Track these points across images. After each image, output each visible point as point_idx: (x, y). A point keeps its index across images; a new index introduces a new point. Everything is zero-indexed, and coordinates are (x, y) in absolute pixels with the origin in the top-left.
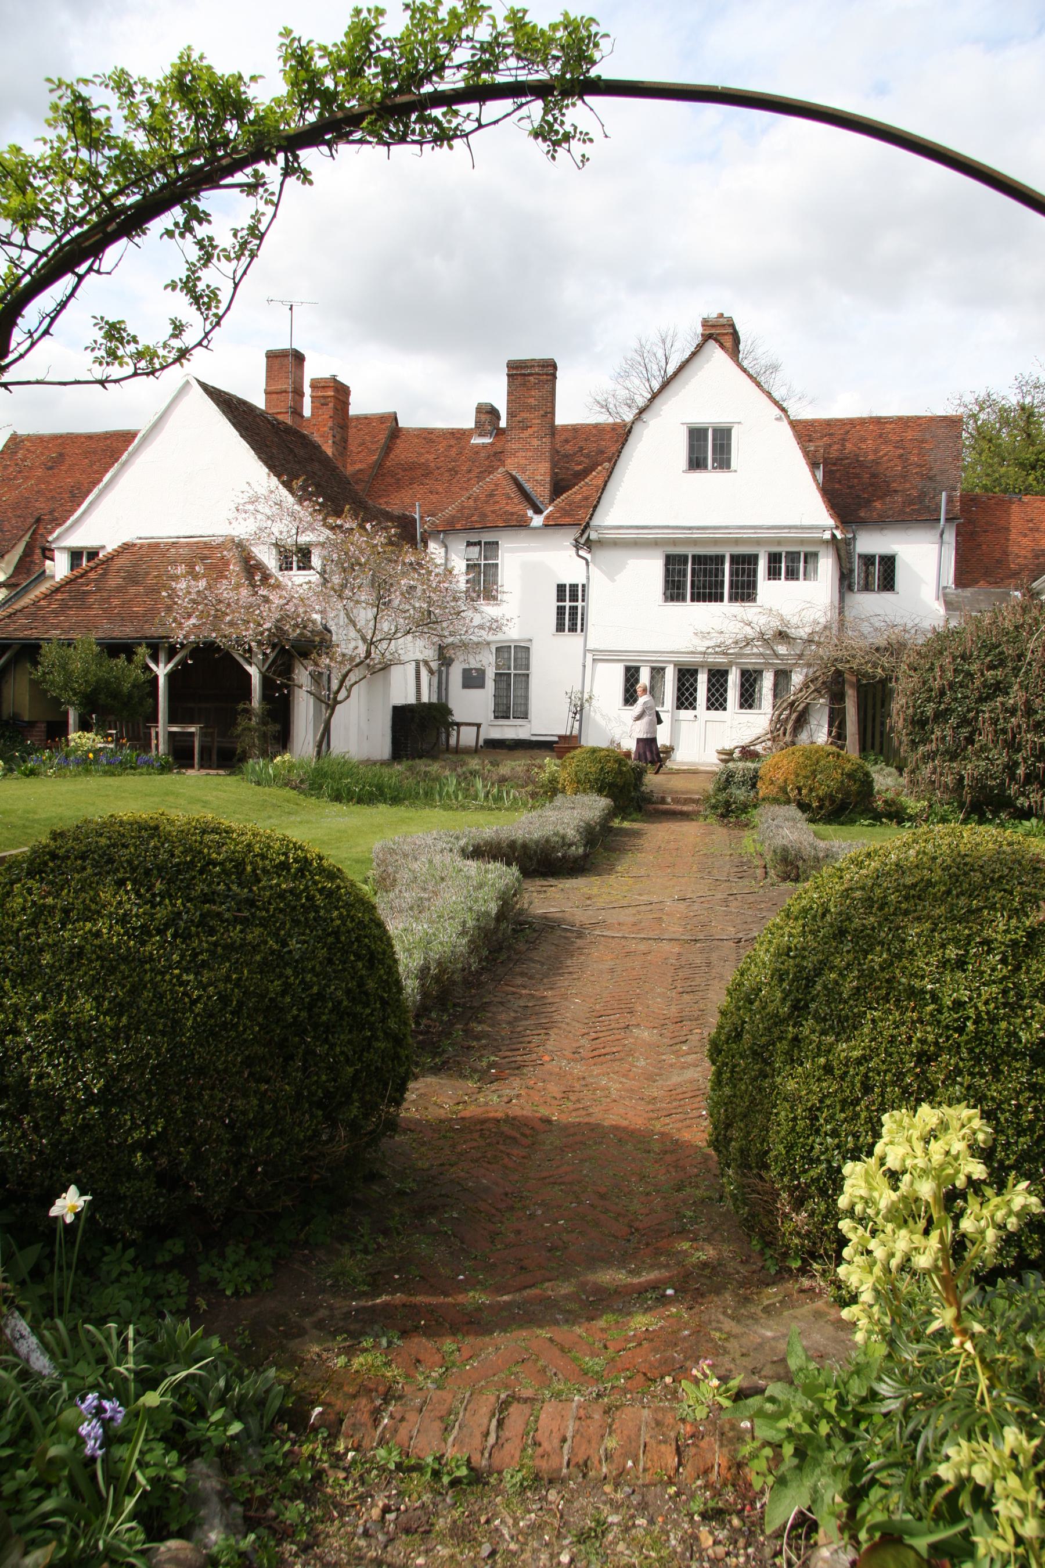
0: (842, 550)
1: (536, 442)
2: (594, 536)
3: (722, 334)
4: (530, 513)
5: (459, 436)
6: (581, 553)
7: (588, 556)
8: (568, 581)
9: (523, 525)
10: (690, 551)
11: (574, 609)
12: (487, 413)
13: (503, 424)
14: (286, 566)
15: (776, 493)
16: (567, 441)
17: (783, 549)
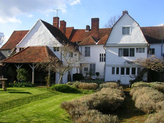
2: (107, 45)
3: (125, 13)
4: (95, 42)
5: (83, 30)
8: (101, 53)
9: (94, 44)
12: (88, 27)
13: (91, 28)
14: (55, 50)
15: (136, 38)
16: (101, 31)
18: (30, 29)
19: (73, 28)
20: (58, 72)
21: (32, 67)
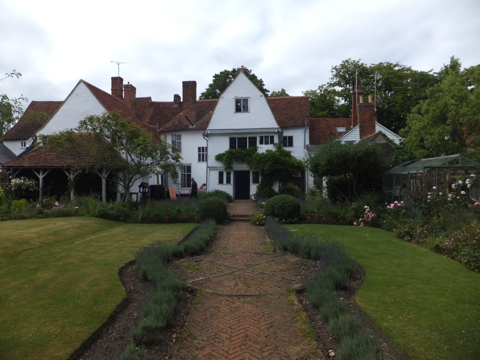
0: (280, 134)
1: (191, 106)
5: (170, 104)
6: (205, 138)
7: (207, 139)
8: (201, 146)
10: (237, 136)
11: (203, 155)
12: (177, 97)
13: (182, 100)
17: (264, 135)
18: (63, 99)
19: (150, 98)
20: (121, 186)
21: (70, 174)
